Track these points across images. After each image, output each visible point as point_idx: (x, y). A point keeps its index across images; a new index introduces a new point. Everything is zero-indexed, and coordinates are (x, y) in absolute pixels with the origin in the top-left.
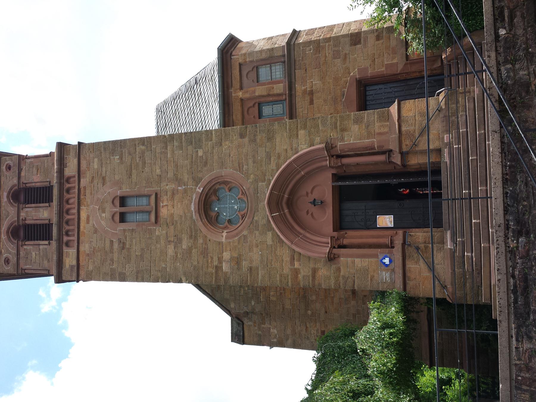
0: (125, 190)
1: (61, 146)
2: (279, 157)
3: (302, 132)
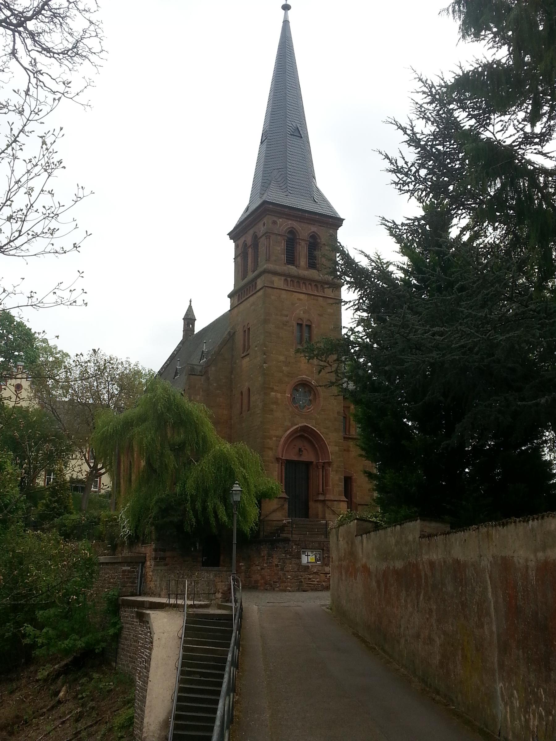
2: (327, 434)
3: (337, 448)
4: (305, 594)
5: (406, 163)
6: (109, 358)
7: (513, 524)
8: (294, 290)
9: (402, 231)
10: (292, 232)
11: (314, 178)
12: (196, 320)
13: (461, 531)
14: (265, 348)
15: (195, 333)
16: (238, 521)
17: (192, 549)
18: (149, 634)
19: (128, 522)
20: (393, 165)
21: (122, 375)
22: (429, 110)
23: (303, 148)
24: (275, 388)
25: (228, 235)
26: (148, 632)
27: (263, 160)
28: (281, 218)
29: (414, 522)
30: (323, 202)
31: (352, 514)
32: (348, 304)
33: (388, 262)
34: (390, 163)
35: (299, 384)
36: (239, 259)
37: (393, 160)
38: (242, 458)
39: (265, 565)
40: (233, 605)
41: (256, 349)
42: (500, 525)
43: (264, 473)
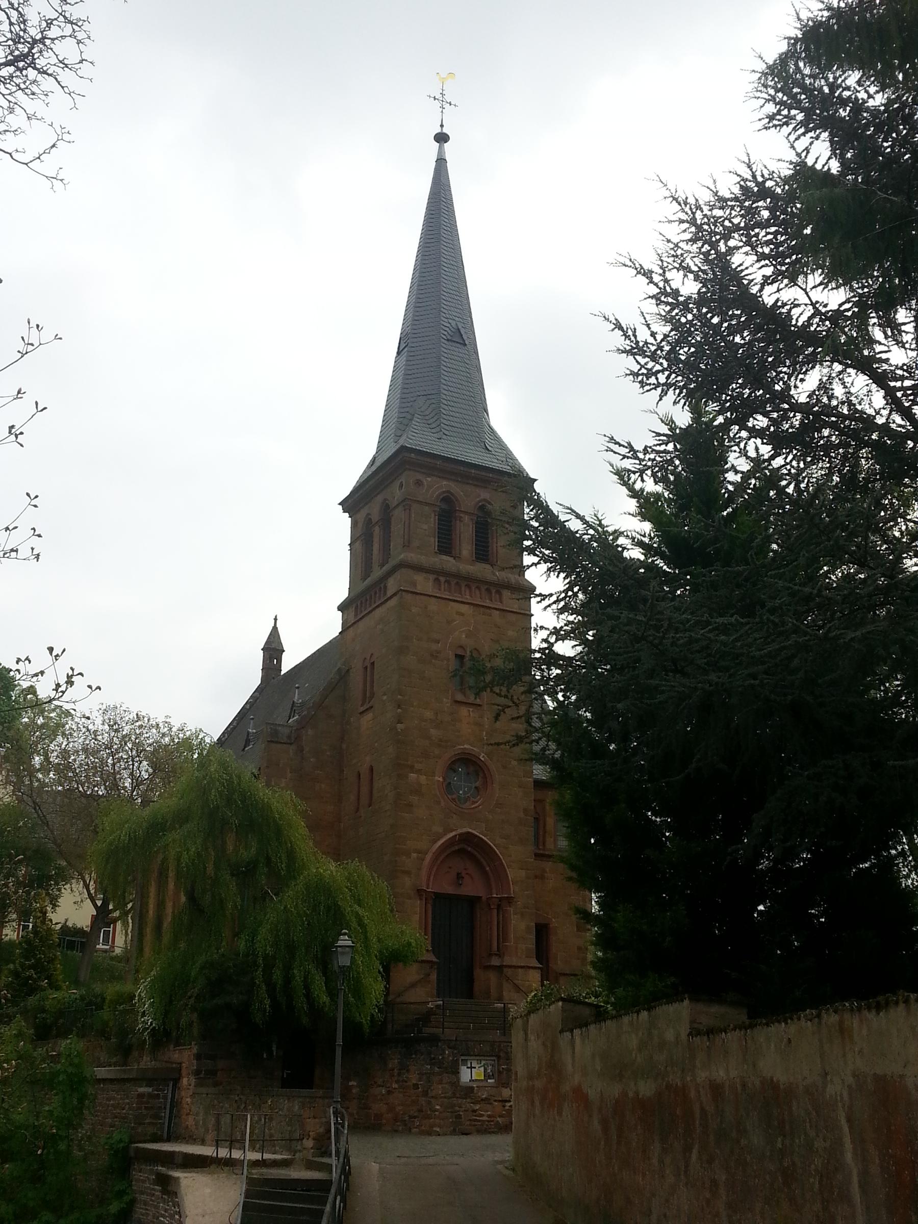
4: (464, 1139)
5: (653, 335)
6: (135, 717)
7: (902, 1006)
8: (451, 598)
9: (644, 463)
10: (448, 499)
11: (486, 411)
12: (284, 651)
13: (779, 1022)
14: (399, 697)
15: (282, 673)
16: (347, 1004)
17: (265, 1056)
18: (177, 1217)
19: (152, 1004)
20: (630, 339)
21: (159, 748)
22: (691, 253)
23: (468, 362)
24: (418, 766)
25: (340, 504)
26: (176, 1213)
27: (400, 381)
28: (429, 475)
29: (676, 1005)
30: (500, 451)
31: (552, 989)
32: (547, 599)
33: (615, 531)
34: (624, 337)
35: (459, 759)
36: (358, 545)
37: (629, 330)
38: (356, 888)
39: (395, 1086)
40: (333, 1161)
41: (385, 698)
42: (869, 1009)
43: (394, 916)
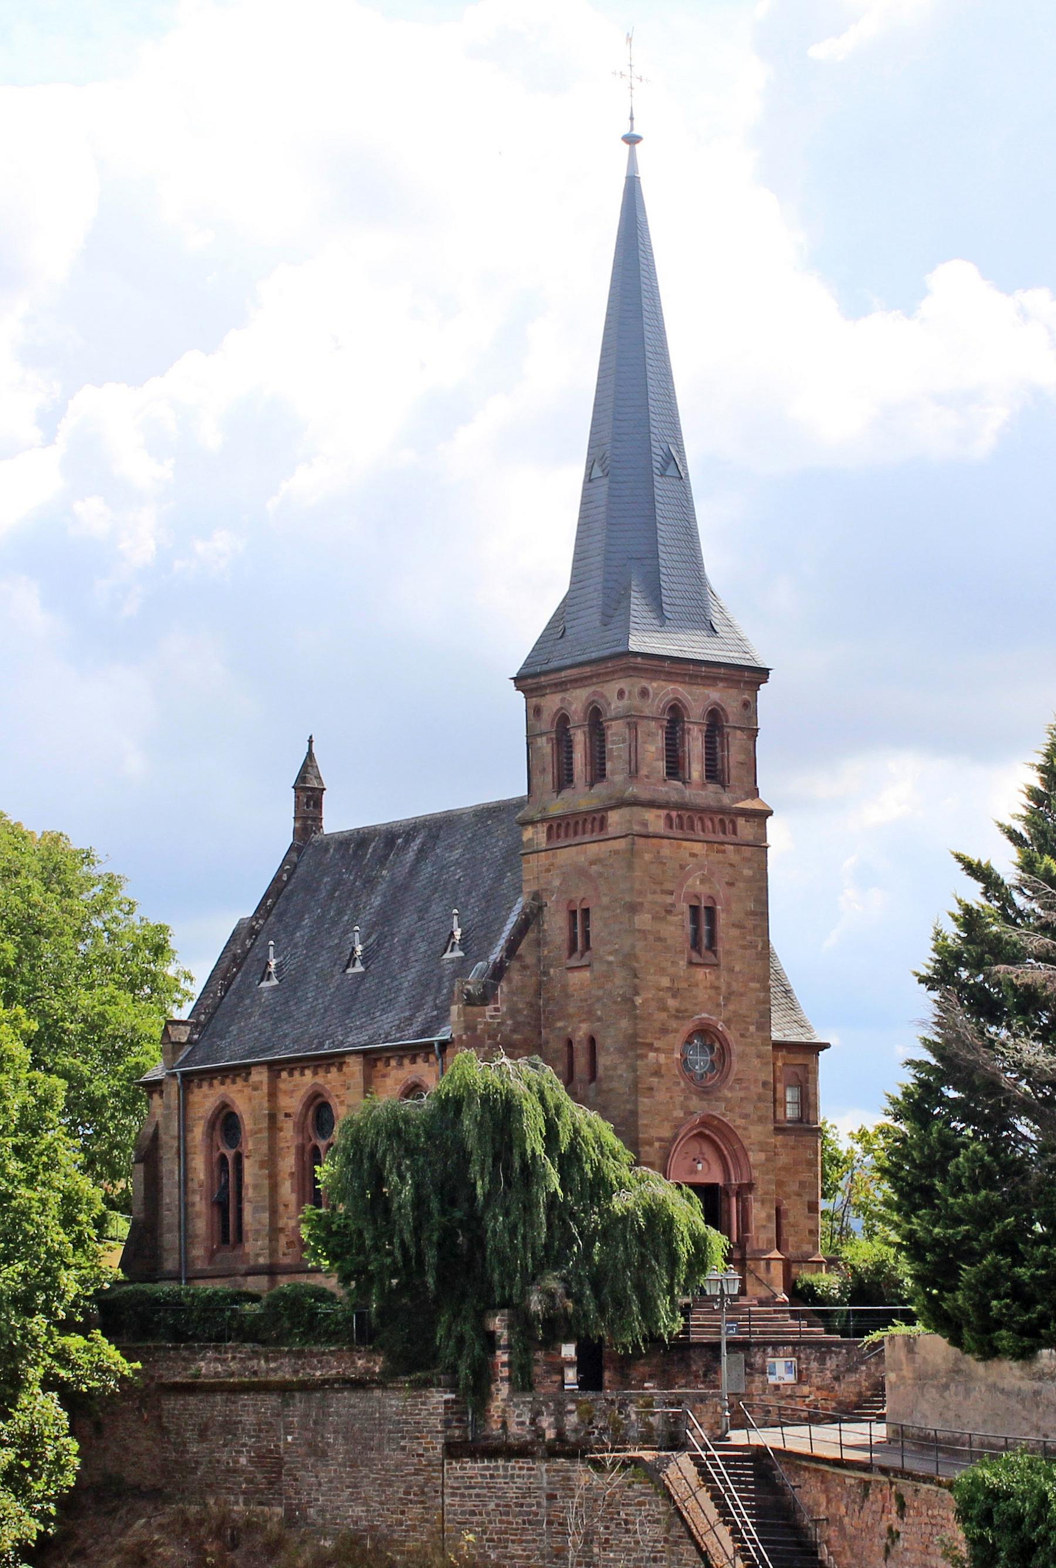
0: (722, 919)
1: (766, 813)
28: (653, 679)
